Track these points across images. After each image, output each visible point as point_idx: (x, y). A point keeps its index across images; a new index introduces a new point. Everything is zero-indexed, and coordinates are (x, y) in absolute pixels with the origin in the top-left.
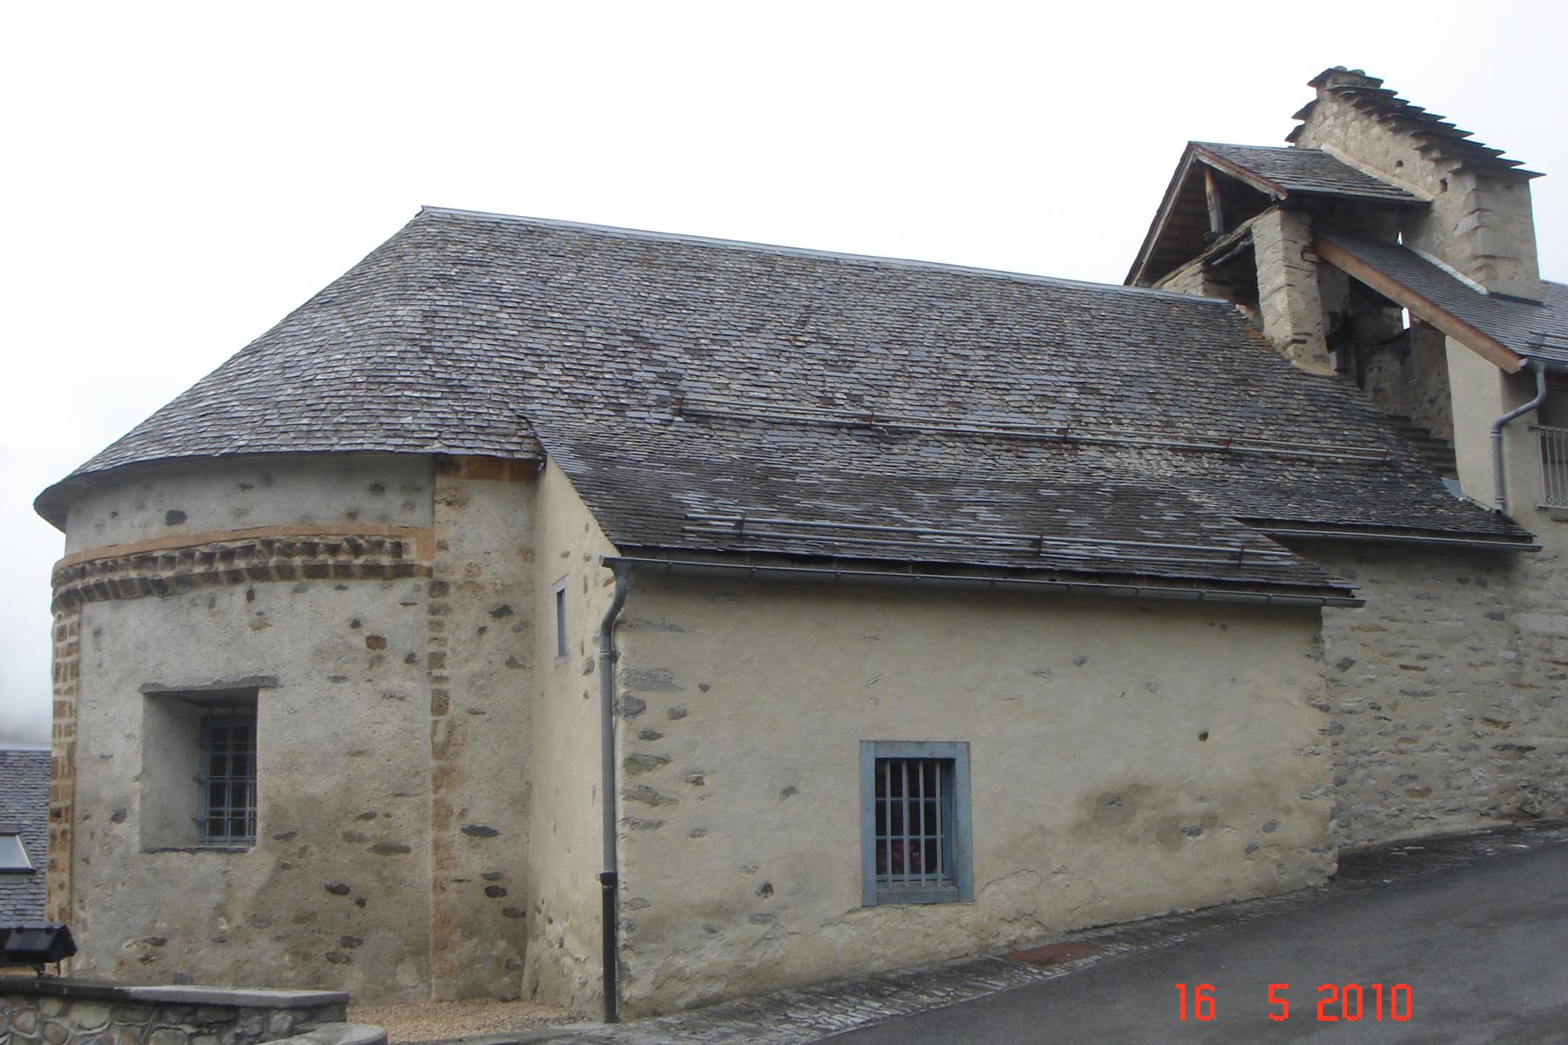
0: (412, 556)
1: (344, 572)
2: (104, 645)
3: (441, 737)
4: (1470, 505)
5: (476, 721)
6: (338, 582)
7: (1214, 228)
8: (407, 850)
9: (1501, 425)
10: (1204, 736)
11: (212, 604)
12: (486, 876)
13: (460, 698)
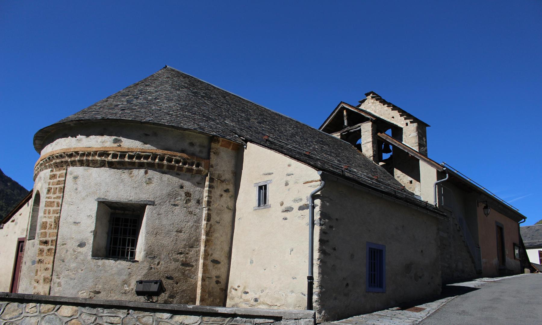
2: (79, 182)
5: (217, 225)
7: (346, 124)
9: (436, 184)
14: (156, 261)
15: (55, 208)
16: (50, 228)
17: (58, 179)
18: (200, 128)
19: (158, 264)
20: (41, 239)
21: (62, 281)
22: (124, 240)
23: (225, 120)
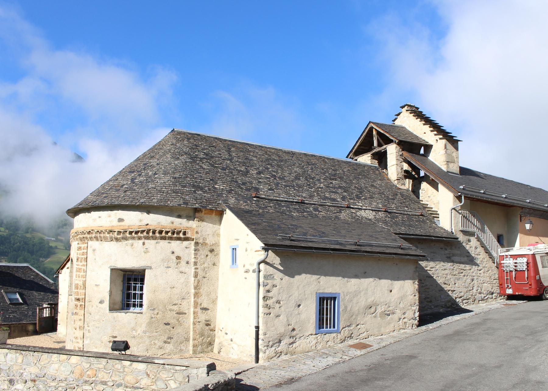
0: (189, 235)
1: (171, 238)
3: (196, 284)
4: (442, 228)
6: (168, 241)
8: (185, 314)
10: (391, 291)
11: (132, 245)
12: (206, 321)
13: (201, 273)
14: (156, 312)
15: (82, 273)
16: (81, 289)
17: (83, 251)
18: (184, 203)
19: (158, 313)
20: (76, 297)
21: (91, 328)
22: (135, 294)
23: (216, 183)
